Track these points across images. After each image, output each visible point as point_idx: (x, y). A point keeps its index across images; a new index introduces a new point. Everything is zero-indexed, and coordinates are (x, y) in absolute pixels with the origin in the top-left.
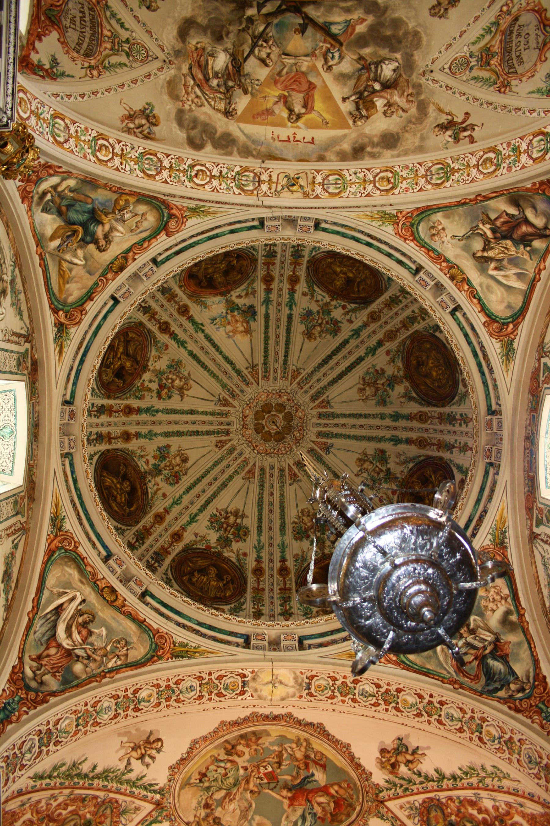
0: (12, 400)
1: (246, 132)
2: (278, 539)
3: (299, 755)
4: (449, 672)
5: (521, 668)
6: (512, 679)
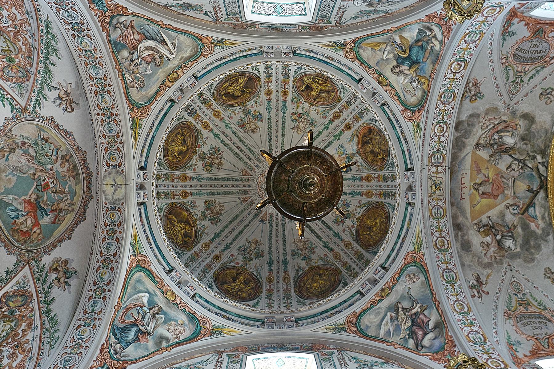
0: (299, 13)
1: (466, 157)
2: (205, 191)
3: (62, 205)
4: (125, 302)
5: (131, 351)
6: (123, 345)
